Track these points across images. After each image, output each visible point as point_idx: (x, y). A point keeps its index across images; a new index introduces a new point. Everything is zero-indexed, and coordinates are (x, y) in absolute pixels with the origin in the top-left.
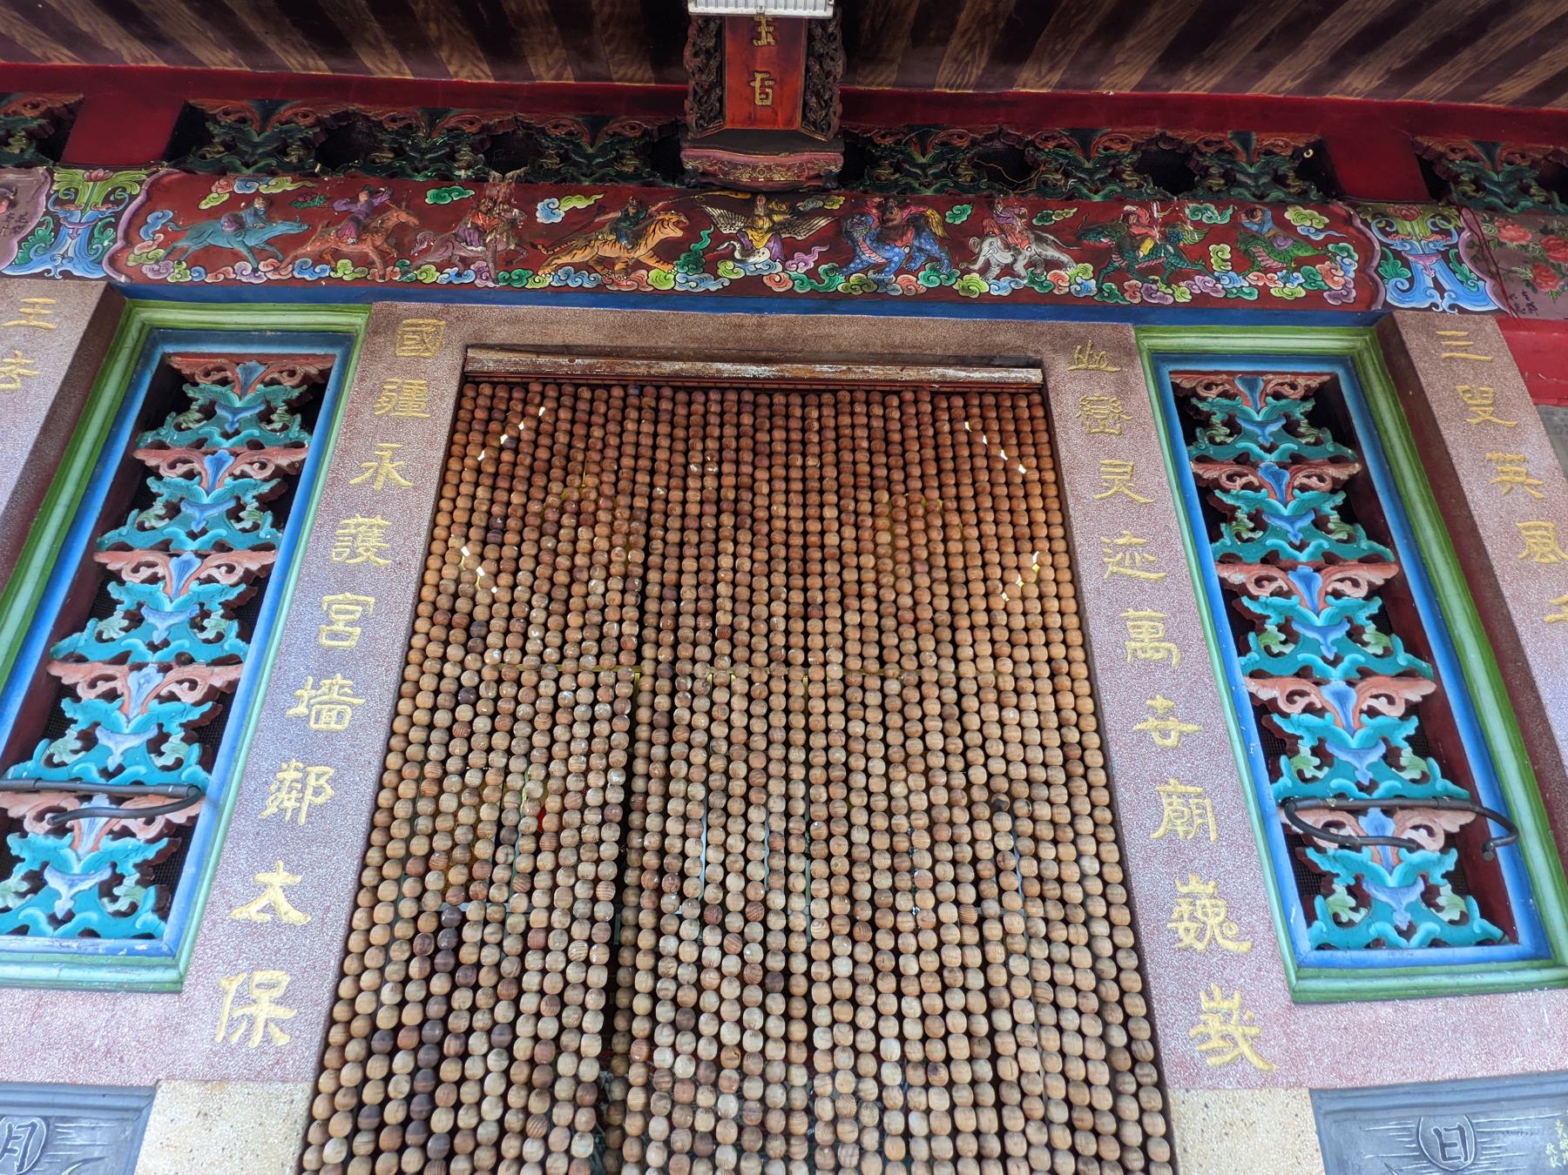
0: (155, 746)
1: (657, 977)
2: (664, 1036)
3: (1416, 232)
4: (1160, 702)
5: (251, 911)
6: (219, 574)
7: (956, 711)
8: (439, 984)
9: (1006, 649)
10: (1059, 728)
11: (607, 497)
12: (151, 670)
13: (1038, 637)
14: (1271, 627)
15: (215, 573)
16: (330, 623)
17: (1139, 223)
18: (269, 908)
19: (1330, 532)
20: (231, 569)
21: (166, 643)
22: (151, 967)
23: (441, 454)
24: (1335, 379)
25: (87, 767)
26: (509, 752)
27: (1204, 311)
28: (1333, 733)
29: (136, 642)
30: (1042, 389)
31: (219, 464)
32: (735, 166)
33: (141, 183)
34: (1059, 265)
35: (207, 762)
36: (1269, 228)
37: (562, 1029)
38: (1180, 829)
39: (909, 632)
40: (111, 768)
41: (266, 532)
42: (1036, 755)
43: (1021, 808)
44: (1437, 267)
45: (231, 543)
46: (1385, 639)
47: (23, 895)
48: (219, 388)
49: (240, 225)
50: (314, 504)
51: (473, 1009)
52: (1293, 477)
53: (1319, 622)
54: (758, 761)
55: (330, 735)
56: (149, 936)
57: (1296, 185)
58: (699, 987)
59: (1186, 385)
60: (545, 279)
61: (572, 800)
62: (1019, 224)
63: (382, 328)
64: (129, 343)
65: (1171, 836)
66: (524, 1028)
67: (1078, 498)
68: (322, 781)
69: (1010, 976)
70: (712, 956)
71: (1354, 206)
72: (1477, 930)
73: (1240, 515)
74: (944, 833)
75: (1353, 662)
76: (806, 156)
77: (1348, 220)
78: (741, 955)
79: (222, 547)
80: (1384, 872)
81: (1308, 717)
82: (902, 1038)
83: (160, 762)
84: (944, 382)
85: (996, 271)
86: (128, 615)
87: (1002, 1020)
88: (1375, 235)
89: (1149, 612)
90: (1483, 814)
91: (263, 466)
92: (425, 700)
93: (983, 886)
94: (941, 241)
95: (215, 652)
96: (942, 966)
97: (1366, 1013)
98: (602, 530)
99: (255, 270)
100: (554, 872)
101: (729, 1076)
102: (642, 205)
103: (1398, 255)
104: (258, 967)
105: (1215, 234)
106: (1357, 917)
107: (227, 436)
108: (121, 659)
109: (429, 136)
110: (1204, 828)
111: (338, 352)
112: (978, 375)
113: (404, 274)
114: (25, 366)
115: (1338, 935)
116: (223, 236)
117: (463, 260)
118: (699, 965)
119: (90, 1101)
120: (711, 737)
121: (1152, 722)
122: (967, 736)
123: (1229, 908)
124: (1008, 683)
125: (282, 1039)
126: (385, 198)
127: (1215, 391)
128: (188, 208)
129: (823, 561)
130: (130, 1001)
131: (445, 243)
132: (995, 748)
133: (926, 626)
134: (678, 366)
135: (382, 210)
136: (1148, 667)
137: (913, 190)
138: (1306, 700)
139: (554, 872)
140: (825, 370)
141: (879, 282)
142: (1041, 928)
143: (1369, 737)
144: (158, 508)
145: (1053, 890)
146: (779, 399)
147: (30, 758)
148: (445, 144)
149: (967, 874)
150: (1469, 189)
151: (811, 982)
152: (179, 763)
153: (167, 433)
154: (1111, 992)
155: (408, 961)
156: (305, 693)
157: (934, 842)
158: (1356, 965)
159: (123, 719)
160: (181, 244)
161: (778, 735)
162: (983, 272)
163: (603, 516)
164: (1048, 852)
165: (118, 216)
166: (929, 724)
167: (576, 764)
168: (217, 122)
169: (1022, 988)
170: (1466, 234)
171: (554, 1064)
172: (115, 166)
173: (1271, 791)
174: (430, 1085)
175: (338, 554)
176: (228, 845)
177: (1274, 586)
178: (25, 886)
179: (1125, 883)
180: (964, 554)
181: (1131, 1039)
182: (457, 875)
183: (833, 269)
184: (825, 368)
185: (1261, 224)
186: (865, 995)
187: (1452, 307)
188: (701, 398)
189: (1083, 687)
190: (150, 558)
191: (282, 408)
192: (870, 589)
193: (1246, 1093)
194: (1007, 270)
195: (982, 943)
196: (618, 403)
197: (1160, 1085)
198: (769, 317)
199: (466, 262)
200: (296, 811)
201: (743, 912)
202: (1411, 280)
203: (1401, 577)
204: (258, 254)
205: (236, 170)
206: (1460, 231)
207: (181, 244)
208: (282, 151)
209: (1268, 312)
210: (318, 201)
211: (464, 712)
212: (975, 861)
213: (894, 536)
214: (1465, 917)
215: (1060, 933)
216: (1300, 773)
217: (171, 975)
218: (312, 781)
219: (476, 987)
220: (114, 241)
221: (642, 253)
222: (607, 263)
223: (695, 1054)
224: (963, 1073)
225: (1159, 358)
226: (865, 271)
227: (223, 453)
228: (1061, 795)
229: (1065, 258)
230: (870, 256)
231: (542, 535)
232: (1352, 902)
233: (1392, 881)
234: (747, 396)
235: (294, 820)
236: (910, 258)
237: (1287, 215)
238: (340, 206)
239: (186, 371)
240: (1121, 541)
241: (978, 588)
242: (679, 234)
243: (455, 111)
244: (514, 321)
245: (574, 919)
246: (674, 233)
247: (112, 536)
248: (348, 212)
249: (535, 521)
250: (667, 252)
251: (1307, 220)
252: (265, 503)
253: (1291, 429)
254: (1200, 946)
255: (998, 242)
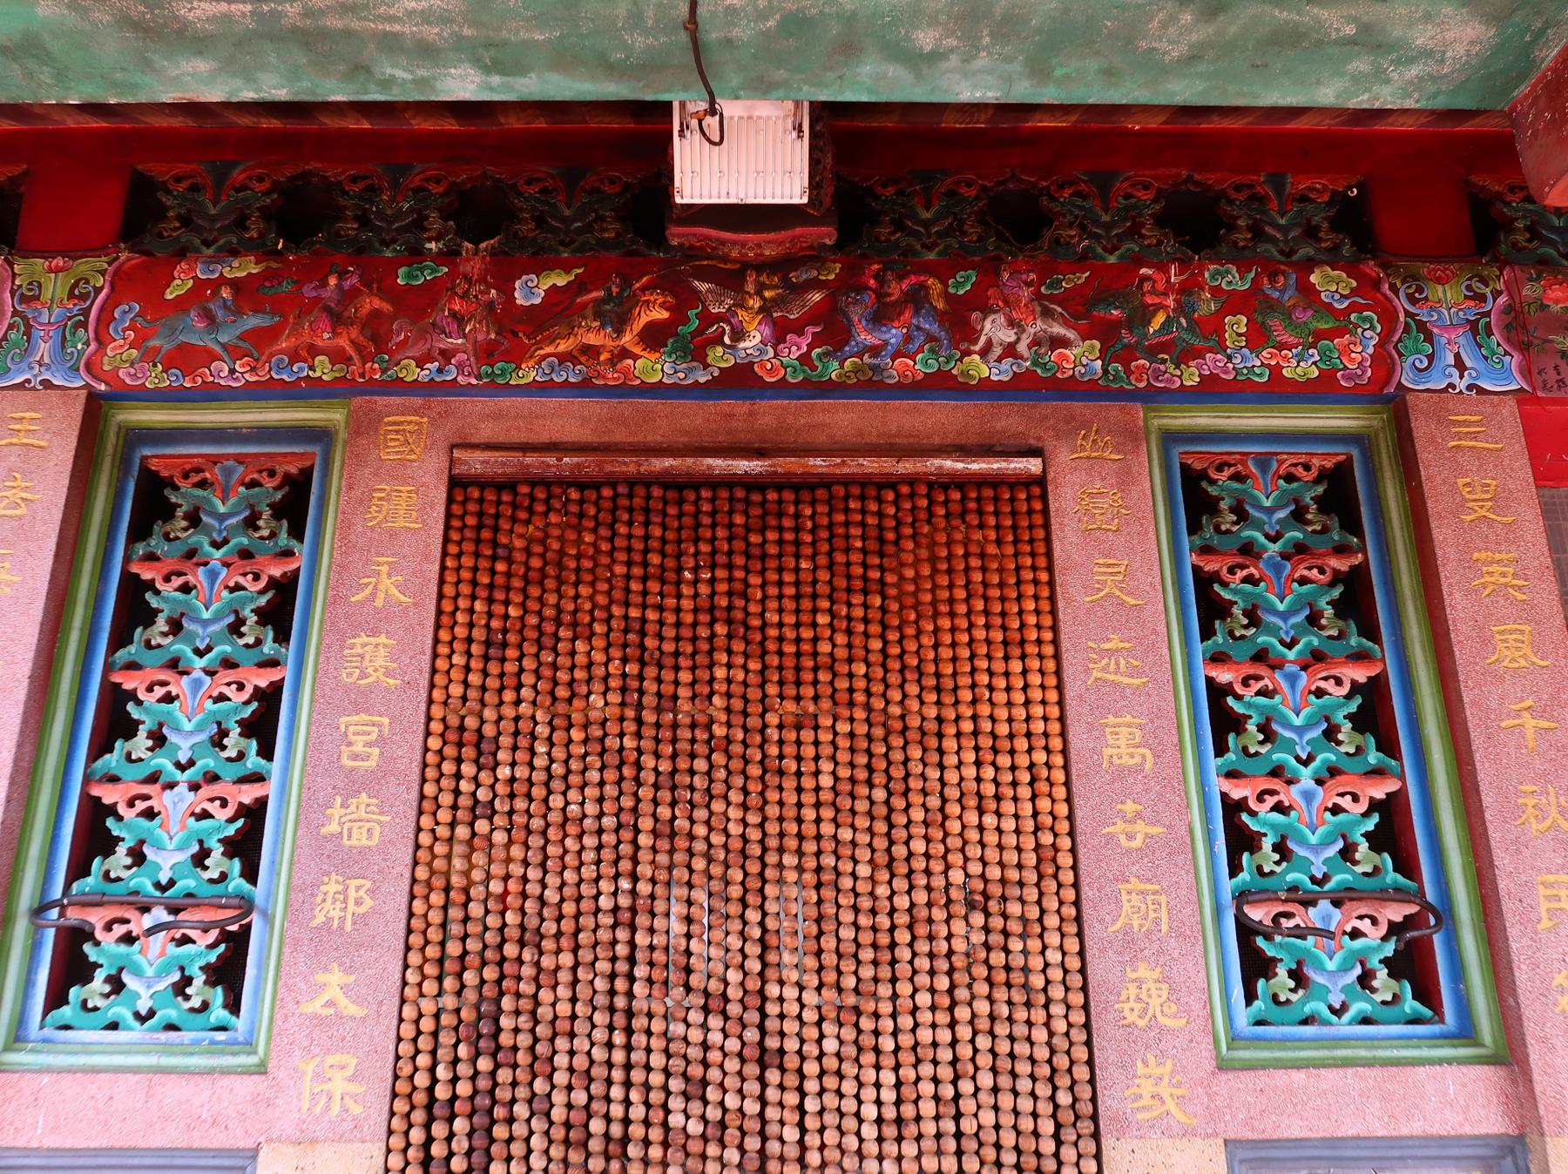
0: (200, 859)
1: (669, 1056)
2: (676, 1103)
3: (1447, 300)
4: (1130, 807)
5: (316, 1006)
6: (230, 692)
7: (939, 818)
8: (484, 1064)
9: (989, 757)
10: (1035, 833)
11: (602, 608)
12: (182, 789)
13: (1021, 744)
14: (1251, 727)
15: (227, 691)
16: (350, 744)
17: (1154, 292)
18: (330, 1003)
19: (1322, 628)
20: (241, 687)
21: (191, 763)
22: (235, 1054)
23: (437, 567)
24: (1350, 459)
25: (142, 882)
26: (526, 863)
27: (1213, 390)
28: (1296, 830)
29: (163, 762)
30: (1041, 481)
31: (213, 576)
32: (723, 242)
33: (103, 272)
34: (1063, 342)
35: (251, 874)
36: (1289, 296)
37: (591, 1098)
38: (1136, 924)
39: (897, 741)
40: (164, 882)
41: (269, 648)
42: (1011, 857)
43: (993, 906)
44: (1462, 341)
45: (237, 658)
46: (1358, 738)
47: (107, 996)
48: (199, 492)
49: (209, 317)
50: (315, 613)
51: (514, 1084)
52: (1294, 569)
53: (1298, 721)
54: (753, 868)
55: (363, 851)
56: (223, 1028)
57: (1328, 238)
58: (706, 1064)
59: (1198, 466)
60: (529, 374)
61: (586, 905)
62: (1026, 293)
63: (363, 426)
64: (110, 449)
65: (1127, 931)
66: (559, 1098)
67: (1069, 602)
68: (362, 893)
69: (976, 1050)
70: (715, 1038)
71: (1385, 266)
72: (1408, 1010)
73: (1236, 611)
74: (922, 930)
75: (1325, 761)
76: (798, 230)
77: (1377, 284)
78: (740, 1037)
79: (229, 664)
80: (1325, 957)
81: (1275, 816)
82: (879, 1103)
83: (207, 875)
84: (941, 472)
85: (998, 351)
86: (151, 735)
87: (966, 1087)
88: (1401, 303)
89: (1129, 719)
90: (1427, 907)
91: (257, 577)
92: (444, 816)
93: (956, 976)
94: (941, 317)
95: (238, 770)
96: (917, 1044)
97: (1280, 1078)
98: (599, 643)
99: (232, 371)
100: (574, 969)
101: (732, 1134)
102: (627, 282)
103: (1422, 327)
104: (328, 1052)
105: (1233, 303)
106: (1294, 997)
107: (217, 545)
108: (153, 778)
109: (392, 200)
110: (1157, 922)
111: (316, 449)
112: (977, 466)
113: (384, 371)
114: (26, 489)
115: (1275, 1013)
116: (194, 333)
117: (443, 352)
118: (705, 1046)
119: (202, 1162)
120: (710, 846)
121: (1120, 825)
122: (949, 840)
123: (1172, 991)
124: (989, 790)
125: (357, 1110)
126: (355, 280)
127: (1227, 473)
128: (156, 307)
129: (815, 669)
130: (227, 1081)
131: (423, 335)
132: (974, 851)
133: (913, 735)
134: (668, 462)
135: (349, 296)
136: (1121, 773)
137: (915, 253)
138: (1275, 799)
139: (574, 969)
140: (818, 464)
141: (874, 368)
142: (1004, 1011)
143: (1328, 834)
144: (161, 624)
145: (1017, 978)
146: (772, 496)
147: (88, 874)
148: (411, 210)
149: (943, 965)
150: (1521, 238)
151: (803, 1058)
152: (223, 877)
153: (156, 543)
154: (1062, 1061)
155: (455, 1046)
156: (336, 812)
157: (914, 938)
158: (1284, 1041)
159: (165, 836)
160: (154, 343)
161: (773, 843)
162: (984, 353)
163: (599, 628)
164: (1016, 945)
165: (86, 312)
166: (914, 830)
167: (588, 872)
168: (169, 192)
169: (984, 1060)
170: (1503, 299)
171: (586, 1126)
172: (75, 251)
173: (1228, 886)
174: (485, 1143)
175: (348, 676)
176: (287, 950)
177: (1260, 684)
178: (107, 989)
179: (1083, 971)
180: (954, 659)
181: (1075, 1100)
182: (490, 973)
183: (826, 354)
184: (819, 462)
185: (1283, 291)
186: (849, 1069)
187: (1470, 387)
188: (692, 497)
189: (1060, 793)
190: (162, 677)
191: (267, 514)
192: (860, 697)
193: (1168, 1142)
194: (1010, 351)
195: (952, 1025)
196: (608, 505)
197: (1096, 1136)
198: (763, 404)
199: (446, 355)
200: (343, 919)
201: (741, 1001)
202: (1431, 358)
203: (1385, 671)
204: (234, 352)
205: (197, 251)
206: (1496, 294)
207: (154, 343)
208: (241, 224)
209: (1279, 390)
210: (286, 287)
211: (482, 826)
212: (950, 953)
213: (885, 643)
214: (1396, 998)
215: (1021, 1014)
216: (1259, 868)
217: (253, 1060)
218: (352, 893)
219: (515, 1066)
220: (87, 344)
221: (627, 339)
222: (591, 351)
223: (703, 1117)
224: (929, 1128)
225: (1170, 438)
226: (860, 355)
227: (215, 564)
228: (1032, 894)
229: (1071, 335)
230: (865, 338)
231: (541, 648)
232: (1292, 984)
233: (1331, 965)
234: (740, 493)
235: (341, 928)
236: (908, 339)
237: (1313, 278)
238: (309, 291)
239: (165, 474)
240: (1107, 646)
241: (966, 695)
242: (665, 315)
243: (418, 168)
244: (497, 416)
245: (594, 1009)
246: (661, 314)
247: (122, 655)
248: (318, 299)
249: (533, 635)
250: (654, 338)
251: (1330, 283)
252: (264, 617)
253: (1299, 516)
254: (1141, 1023)
255: (1001, 319)
